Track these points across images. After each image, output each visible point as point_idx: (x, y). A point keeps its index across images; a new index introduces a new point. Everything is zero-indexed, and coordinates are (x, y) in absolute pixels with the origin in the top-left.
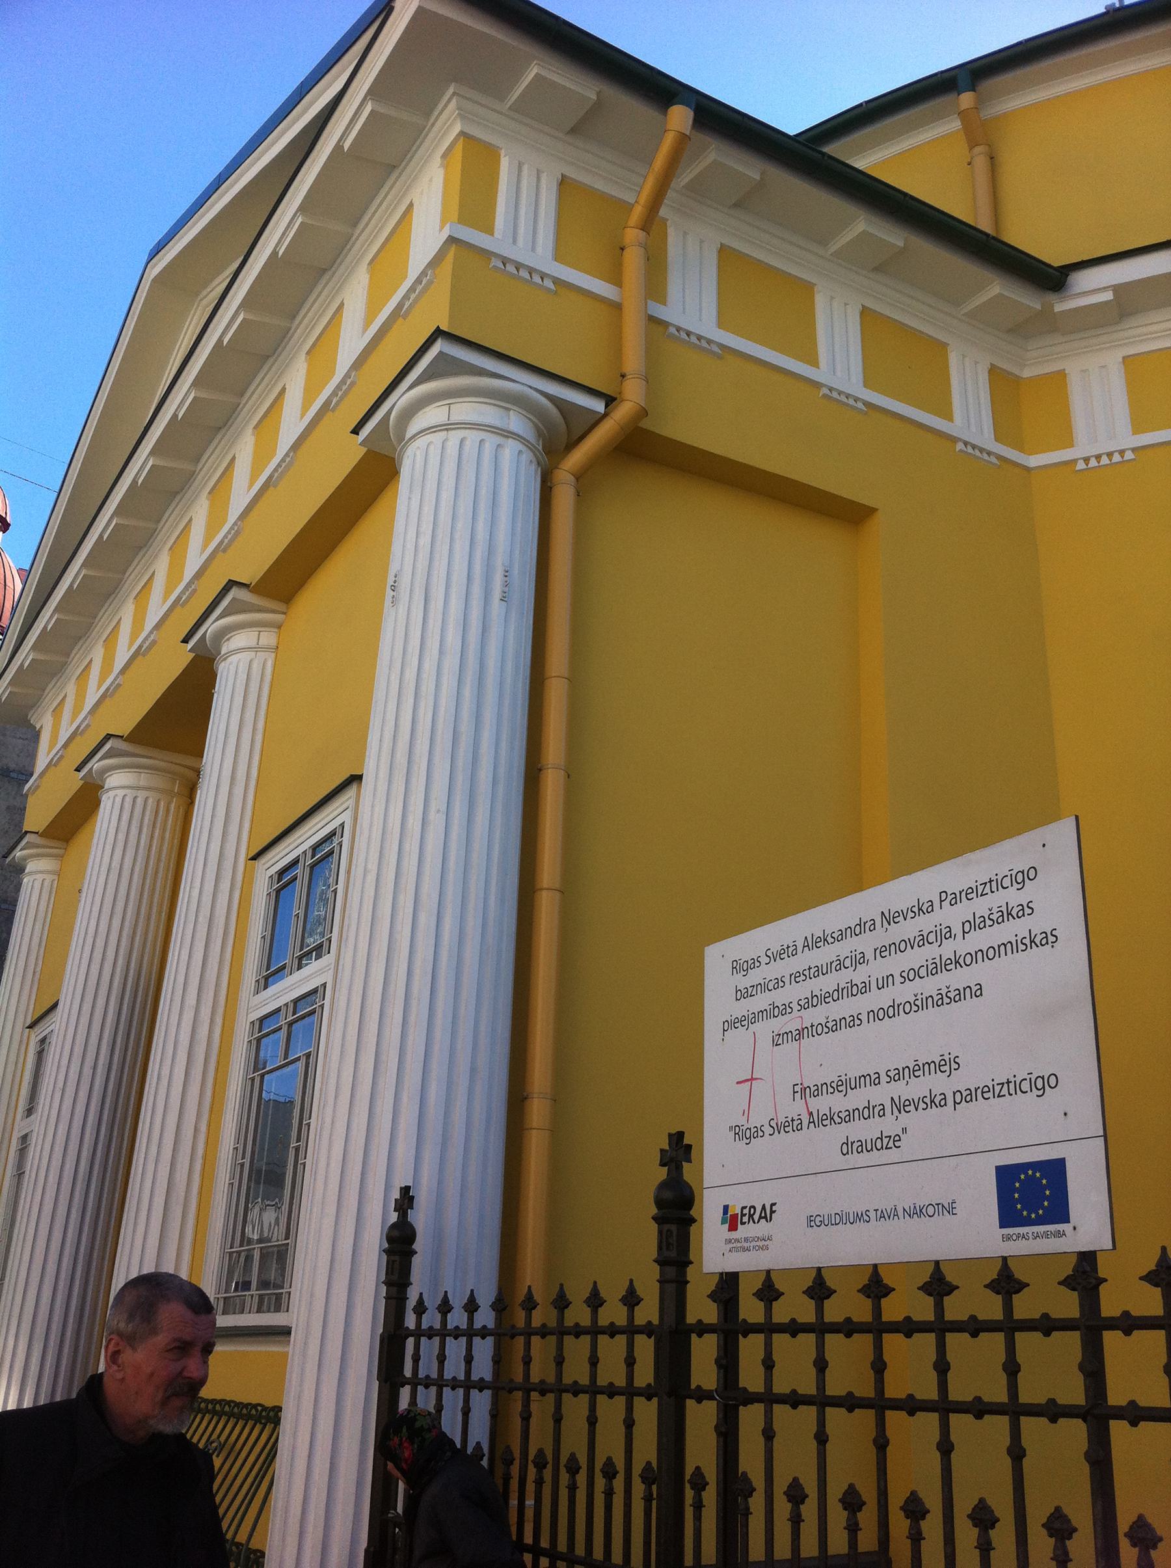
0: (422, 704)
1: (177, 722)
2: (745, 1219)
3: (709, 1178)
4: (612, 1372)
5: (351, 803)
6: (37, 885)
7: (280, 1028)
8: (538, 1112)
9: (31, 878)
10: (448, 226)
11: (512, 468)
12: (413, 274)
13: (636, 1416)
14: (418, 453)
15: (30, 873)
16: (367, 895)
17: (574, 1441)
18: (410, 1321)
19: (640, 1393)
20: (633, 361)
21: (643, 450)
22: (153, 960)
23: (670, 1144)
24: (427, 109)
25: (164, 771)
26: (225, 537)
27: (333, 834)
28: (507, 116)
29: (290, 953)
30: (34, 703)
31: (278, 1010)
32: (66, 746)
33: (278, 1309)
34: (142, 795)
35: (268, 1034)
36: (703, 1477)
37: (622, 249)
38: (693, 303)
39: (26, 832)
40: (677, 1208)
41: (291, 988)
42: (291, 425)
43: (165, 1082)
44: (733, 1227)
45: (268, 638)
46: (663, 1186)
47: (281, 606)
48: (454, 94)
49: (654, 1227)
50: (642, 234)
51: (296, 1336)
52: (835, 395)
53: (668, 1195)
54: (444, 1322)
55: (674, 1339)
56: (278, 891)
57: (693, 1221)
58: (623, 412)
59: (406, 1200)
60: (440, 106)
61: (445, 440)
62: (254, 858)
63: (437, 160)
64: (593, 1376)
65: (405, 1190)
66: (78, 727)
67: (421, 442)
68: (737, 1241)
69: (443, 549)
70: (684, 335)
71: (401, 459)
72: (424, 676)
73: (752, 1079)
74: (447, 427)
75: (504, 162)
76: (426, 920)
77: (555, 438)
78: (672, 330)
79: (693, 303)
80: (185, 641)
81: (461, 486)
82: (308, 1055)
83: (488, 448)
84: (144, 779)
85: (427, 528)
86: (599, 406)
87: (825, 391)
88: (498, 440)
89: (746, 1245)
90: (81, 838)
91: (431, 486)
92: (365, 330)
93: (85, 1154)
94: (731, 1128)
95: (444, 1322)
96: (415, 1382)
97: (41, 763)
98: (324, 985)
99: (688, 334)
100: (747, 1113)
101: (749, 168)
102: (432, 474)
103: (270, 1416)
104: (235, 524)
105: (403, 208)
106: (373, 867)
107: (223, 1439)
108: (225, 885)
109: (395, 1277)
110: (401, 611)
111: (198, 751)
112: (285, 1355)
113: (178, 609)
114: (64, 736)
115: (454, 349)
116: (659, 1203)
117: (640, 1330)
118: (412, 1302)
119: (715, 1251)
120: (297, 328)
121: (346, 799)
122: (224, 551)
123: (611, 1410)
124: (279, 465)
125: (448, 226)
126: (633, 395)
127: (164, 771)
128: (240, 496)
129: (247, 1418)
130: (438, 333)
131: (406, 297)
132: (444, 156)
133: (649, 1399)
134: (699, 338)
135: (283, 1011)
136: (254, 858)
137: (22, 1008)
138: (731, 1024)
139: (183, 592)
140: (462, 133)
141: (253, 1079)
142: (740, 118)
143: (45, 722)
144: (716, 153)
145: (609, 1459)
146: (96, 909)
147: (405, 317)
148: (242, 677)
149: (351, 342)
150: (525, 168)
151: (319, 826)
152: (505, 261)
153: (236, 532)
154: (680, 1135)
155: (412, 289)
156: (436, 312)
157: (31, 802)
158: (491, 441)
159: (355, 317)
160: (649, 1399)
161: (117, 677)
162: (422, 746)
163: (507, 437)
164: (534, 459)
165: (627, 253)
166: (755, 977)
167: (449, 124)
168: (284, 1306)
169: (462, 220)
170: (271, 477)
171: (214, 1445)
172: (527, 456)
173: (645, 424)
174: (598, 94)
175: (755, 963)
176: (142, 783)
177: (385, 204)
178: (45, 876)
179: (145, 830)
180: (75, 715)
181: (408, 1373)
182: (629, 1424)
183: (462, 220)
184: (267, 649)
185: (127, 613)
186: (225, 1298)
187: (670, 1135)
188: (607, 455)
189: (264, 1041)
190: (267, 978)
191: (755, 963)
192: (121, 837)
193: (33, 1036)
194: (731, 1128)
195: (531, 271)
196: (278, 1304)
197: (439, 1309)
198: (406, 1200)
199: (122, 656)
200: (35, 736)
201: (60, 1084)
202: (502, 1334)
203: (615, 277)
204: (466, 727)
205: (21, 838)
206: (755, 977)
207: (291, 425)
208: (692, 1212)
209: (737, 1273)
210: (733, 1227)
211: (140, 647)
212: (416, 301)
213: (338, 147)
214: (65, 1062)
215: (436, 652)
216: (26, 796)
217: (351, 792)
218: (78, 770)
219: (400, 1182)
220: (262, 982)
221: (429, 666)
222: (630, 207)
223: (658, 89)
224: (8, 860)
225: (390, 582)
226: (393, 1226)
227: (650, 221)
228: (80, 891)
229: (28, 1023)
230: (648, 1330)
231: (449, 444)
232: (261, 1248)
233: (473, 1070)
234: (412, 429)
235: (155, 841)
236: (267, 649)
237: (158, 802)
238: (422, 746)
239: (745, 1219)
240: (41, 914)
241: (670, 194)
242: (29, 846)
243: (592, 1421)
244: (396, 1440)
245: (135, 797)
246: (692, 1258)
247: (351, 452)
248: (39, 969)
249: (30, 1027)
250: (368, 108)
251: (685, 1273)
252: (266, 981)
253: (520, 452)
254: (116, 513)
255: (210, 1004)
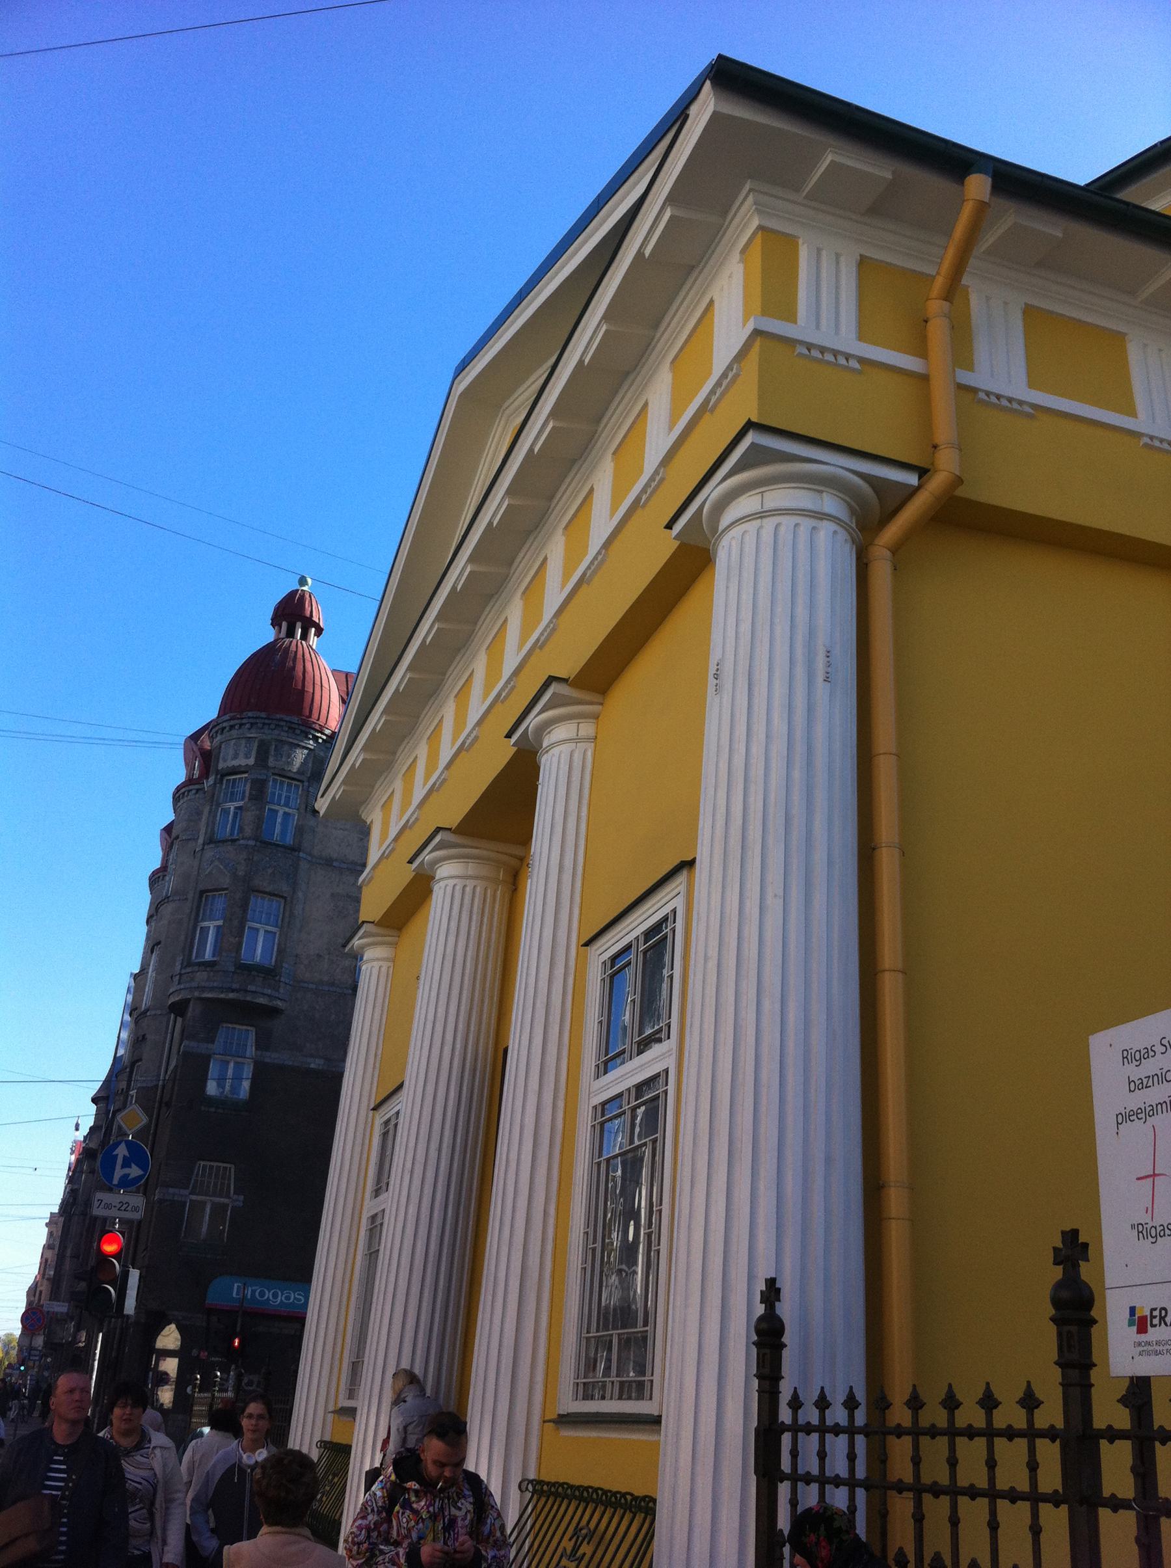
0: (752, 788)
1: (502, 815)
2: (1156, 1321)
3: (1112, 1277)
4: (1012, 1475)
5: (682, 888)
6: (375, 972)
7: (624, 1113)
8: (896, 1201)
9: (369, 965)
10: (752, 319)
11: (827, 550)
12: (718, 367)
13: (1042, 1522)
14: (734, 543)
15: (368, 961)
16: (702, 979)
17: (938, 1540)
18: (785, 1415)
19: (1046, 1498)
20: (944, 429)
21: (965, 520)
22: (487, 1044)
23: (1063, 1242)
24: (724, 208)
25: (488, 859)
26: (542, 634)
27: (665, 919)
28: (804, 205)
29: (628, 1041)
30: (365, 800)
31: (620, 1095)
32: (396, 839)
33: (640, 1397)
34: (470, 884)
35: (610, 1119)
36: (905, 1556)
37: (926, 322)
38: (1002, 365)
39: (363, 922)
40: (1076, 1309)
41: (633, 1072)
42: (601, 524)
43: (513, 1165)
44: (1142, 1329)
45: (587, 729)
46: (1058, 1286)
47: (596, 698)
48: (750, 190)
49: (1053, 1328)
50: (946, 304)
51: (668, 1423)
52: (1157, 443)
53: (1065, 1294)
54: (822, 1418)
55: (1081, 1443)
56: (612, 977)
57: (1095, 1322)
58: (936, 483)
59: (772, 1292)
60: (737, 203)
61: (761, 527)
62: (587, 944)
63: (736, 256)
64: (992, 1479)
65: (771, 1283)
66: (408, 821)
67: (736, 532)
68: (1148, 1343)
69: (764, 635)
70: (993, 399)
71: (716, 545)
72: (753, 761)
73: (1154, 1175)
74: (761, 515)
75: (804, 253)
76: (771, 1005)
77: (870, 513)
78: (982, 395)
79: (1002, 365)
80: (509, 736)
81: (777, 573)
82: (655, 1141)
83: (804, 533)
84: (472, 868)
85: (746, 615)
86: (912, 479)
87: (1146, 440)
88: (812, 522)
89: (1158, 1348)
90: (413, 928)
91: (748, 575)
92: (671, 429)
93: (435, 1233)
94: (1133, 1226)
95: (822, 1418)
96: (795, 1478)
97: (373, 856)
98: (667, 1071)
99: (998, 397)
100: (1150, 1210)
101: (1051, 227)
102: (749, 562)
103: (645, 1507)
104: (551, 622)
105: (704, 305)
106: (713, 953)
107: (592, 1525)
108: (559, 971)
109: (767, 1371)
110: (725, 701)
111: (525, 839)
112: (658, 1443)
113: (499, 704)
114: (393, 832)
115: (765, 443)
116: (1056, 1302)
117: (1042, 1434)
118: (785, 1396)
119: (1122, 1354)
120: (602, 431)
121: (679, 883)
122: (541, 648)
123: (1014, 1516)
124: (592, 563)
125: (752, 319)
126: (947, 464)
127: (488, 859)
128: (553, 595)
129: (565, 1496)
130: (750, 425)
131: (713, 392)
132: (743, 251)
133: (1057, 1506)
134: (1010, 400)
135: (626, 1096)
136: (587, 944)
137: (366, 1094)
138: (1125, 1117)
139: (503, 689)
140: (761, 228)
141: (599, 1164)
142: (1039, 179)
143: (374, 816)
144: (1013, 217)
145: (901, 1549)
146: (434, 994)
147: (712, 411)
148: (564, 768)
149: (657, 440)
150: (824, 253)
151: (651, 911)
152: (810, 346)
153: (552, 629)
154: (1075, 1233)
155: (718, 384)
156: (744, 405)
157: (365, 891)
158: (806, 523)
159: (658, 414)
160: (1057, 1506)
161: (443, 772)
162: (755, 833)
163: (822, 519)
164: (849, 538)
165: (931, 326)
166: (1150, 1067)
167: (747, 220)
168: (647, 1394)
169: (766, 312)
170: (584, 574)
171: (584, 1532)
172: (843, 535)
173: (960, 492)
174: (894, 173)
175: (1149, 1053)
176: (470, 873)
177: (685, 303)
178: (381, 963)
179: (474, 917)
180: (403, 811)
181: (786, 1465)
182: (1036, 1530)
183: (766, 312)
184: (587, 739)
185: (449, 711)
186: (584, 1384)
187: (1063, 1233)
188: (923, 525)
189: (607, 1125)
190: (606, 1063)
191: (1149, 1053)
192: (454, 925)
193: (377, 1117)
194: (1133, 1226)
195: (836, 353)
196: (640, 1390)
197: (816, 1404)
198: (772, 1292)
199: (446, 754)
200: (364, 831)
201: (409, 1165)
202: (878, 1432)
203: (921, 349)
204: (798, 810)
205: (359, 928)
206: (1150, 1067)
207: (601, 524)
208: (1094, 1313)
209: (1149, 1378)
210: (1142, 1329)
211: (464, 743)
212: (723, 394)
213: (640, 254)
214: (412, 1144)
215: (762, 737)
216: (360, 888)
217: (682, 878)
218: (410, 862)
219: (765, 1271)
220: (602, 1067)
221: (757, 750)
222: (931, 278)
223: (954, 161)
224: (347, 949)
225: (712, 670)
226: (761, 1319)
227: (953, 291)
228: (418, 978)
229: (372, 1106)
230: (1051, 1434)
231: (764, 532)
232: (619, 1335)
233: (828, 1160)
234: (726, 520)
235: (484, 927)
236: (587, 739)
237: (486, 889)
238: (755, 833)
239: (1156, 1321)
240: (380, 1000)
241: (972, 261)
242: (366, 935)
243: (954, 1521)
244: (813, 1537)
245: (465, 886)
246: (1095, 1359)
247: (666, 545)
248: (380, 1052)
249: (374, 1109)
250: (668, 214)
251: (1089, 1377)
252: (605, 1067)
253: (835, 532)
254: (437, 619)
255: (552, 1086)
